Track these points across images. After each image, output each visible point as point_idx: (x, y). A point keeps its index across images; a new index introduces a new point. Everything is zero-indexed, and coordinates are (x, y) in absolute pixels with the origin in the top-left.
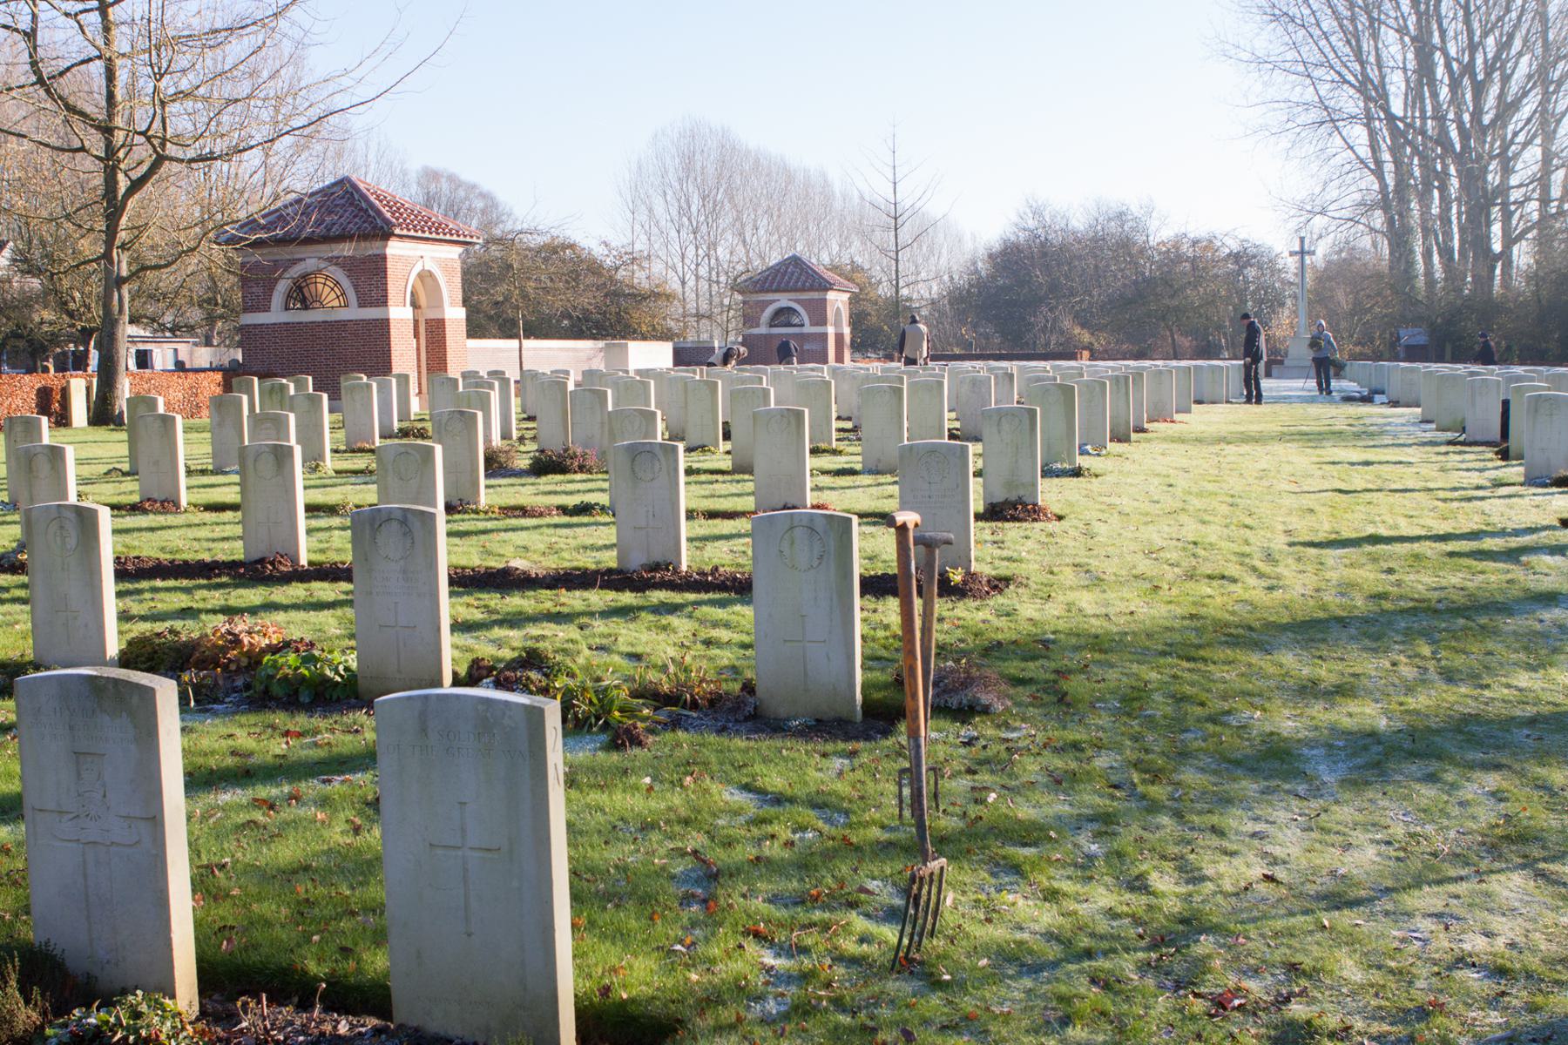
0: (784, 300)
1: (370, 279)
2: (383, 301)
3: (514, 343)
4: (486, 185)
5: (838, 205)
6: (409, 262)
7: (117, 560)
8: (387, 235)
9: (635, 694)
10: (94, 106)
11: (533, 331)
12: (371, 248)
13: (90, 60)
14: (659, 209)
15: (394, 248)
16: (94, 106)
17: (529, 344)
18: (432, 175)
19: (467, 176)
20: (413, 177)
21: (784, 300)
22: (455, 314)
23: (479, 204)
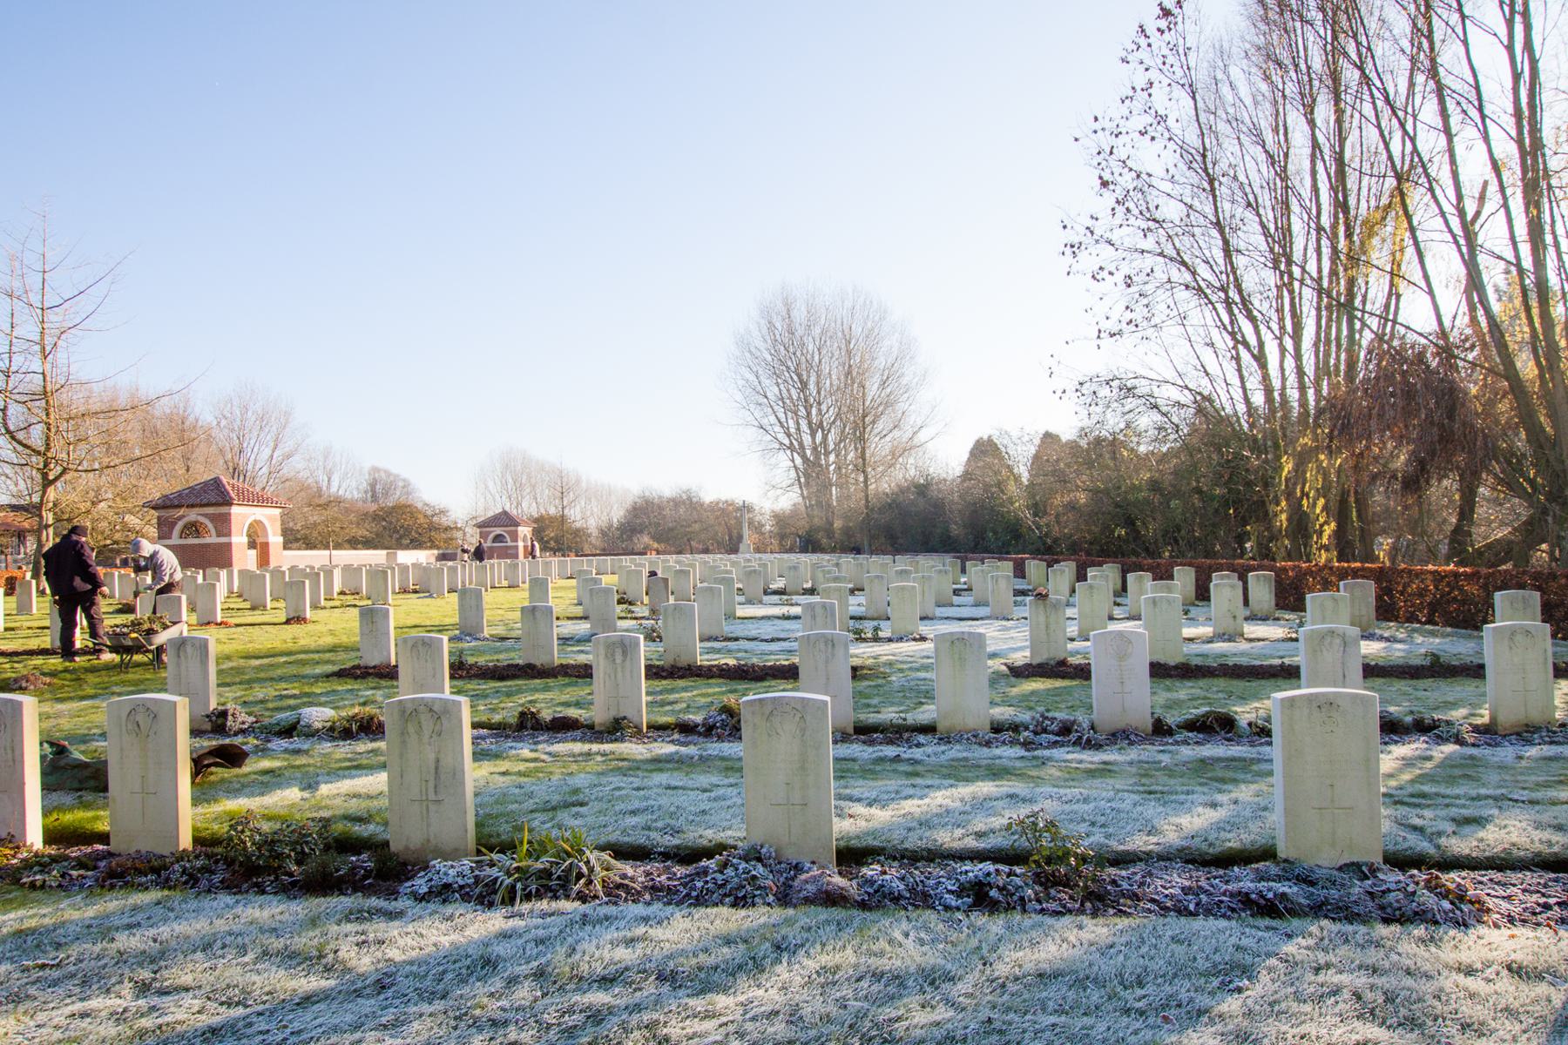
0: (498, 531)
1: (223, 525)
2: (229, 534)
3: (327, 552)
4: (405, 474)
5: (584, 485)
6: (246, 516)
7: (195, 829)
8: (230, 504)
9: (327, 848)
10: (38, 443)
11: (338, 546)
12: (223, 510)
13: (1499, 257)
14: (491, 484)
15: (235, 510)
16: (38, 443)
17: (334, 552)
18: (375, 469)
19: (394, 471)
20: (366, 471)
21: (498, 531)
22: (275, 539)
23: (401, 484)
